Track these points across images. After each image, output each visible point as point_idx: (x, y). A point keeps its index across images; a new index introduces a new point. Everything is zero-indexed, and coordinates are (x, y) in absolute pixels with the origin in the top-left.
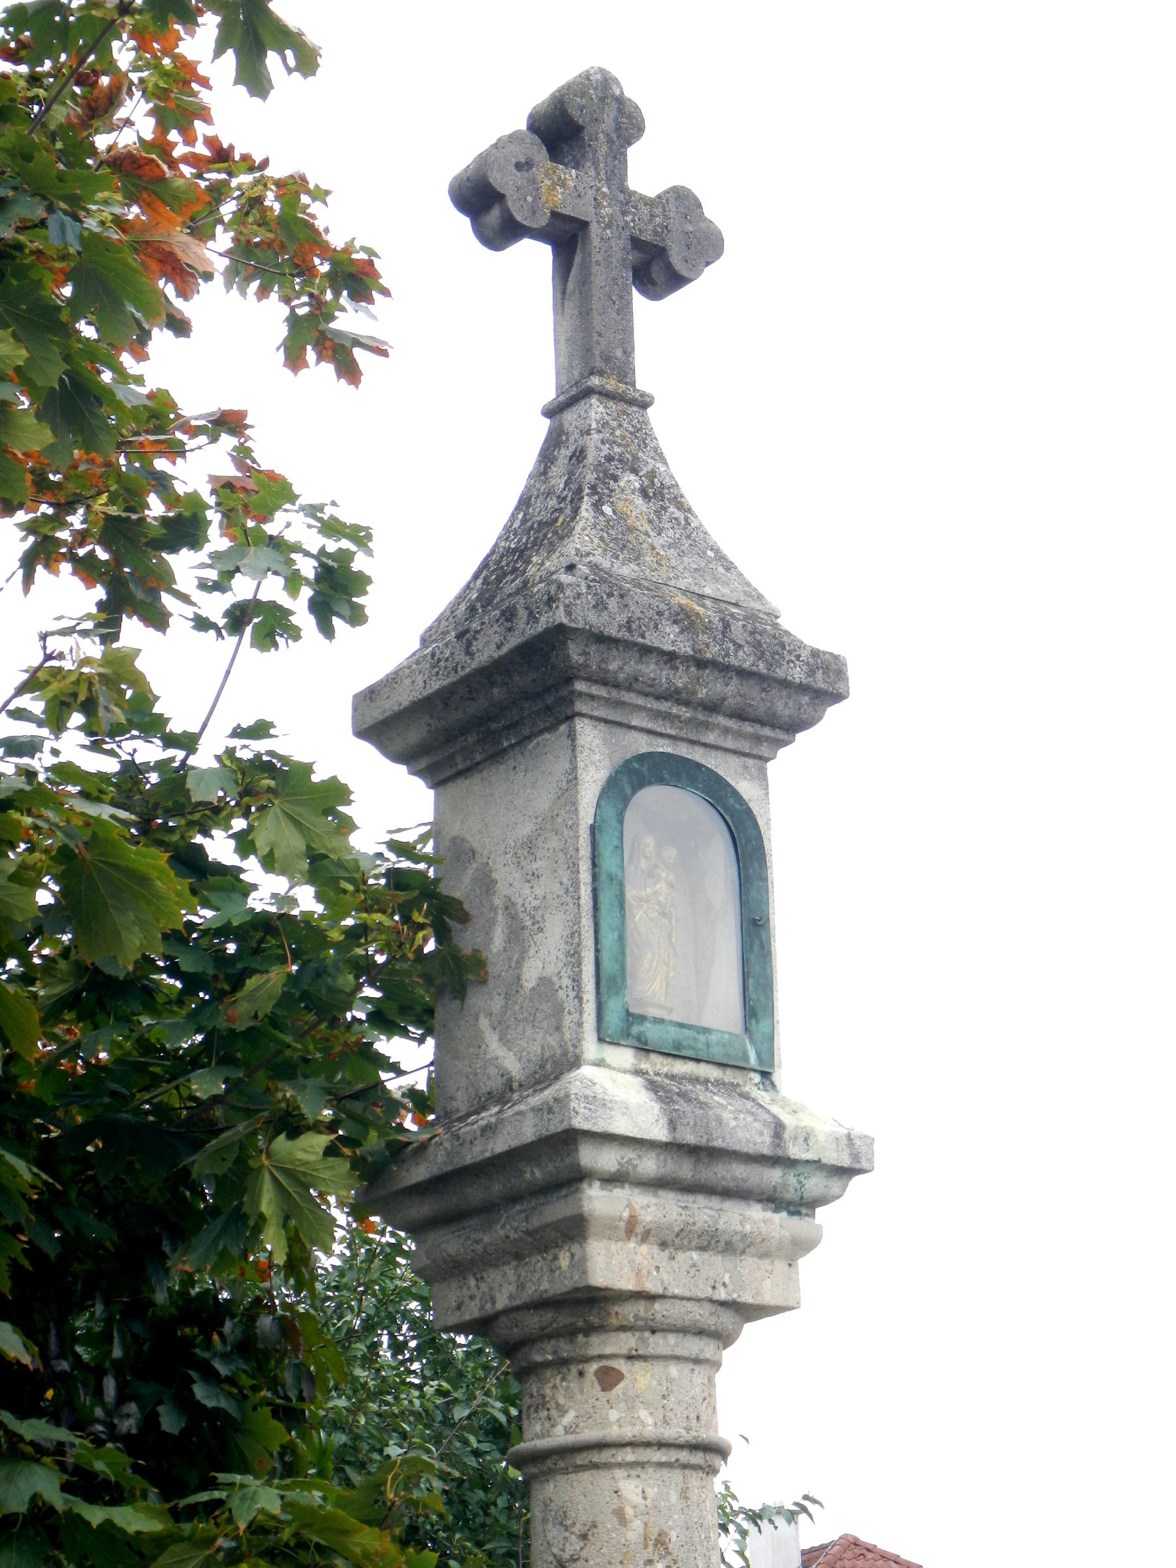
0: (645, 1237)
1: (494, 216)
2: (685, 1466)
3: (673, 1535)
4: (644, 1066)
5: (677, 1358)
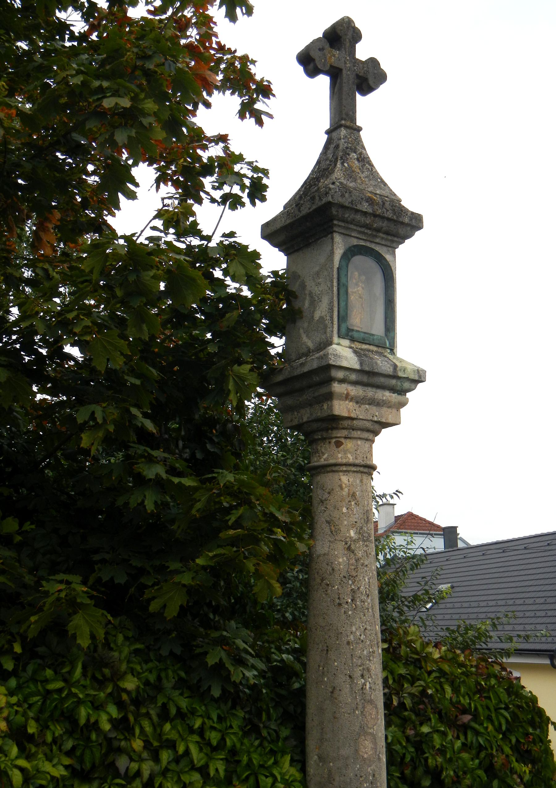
1: (311, 66)
2: (362, 472)
3: (357, 493)
4: (352, 346)
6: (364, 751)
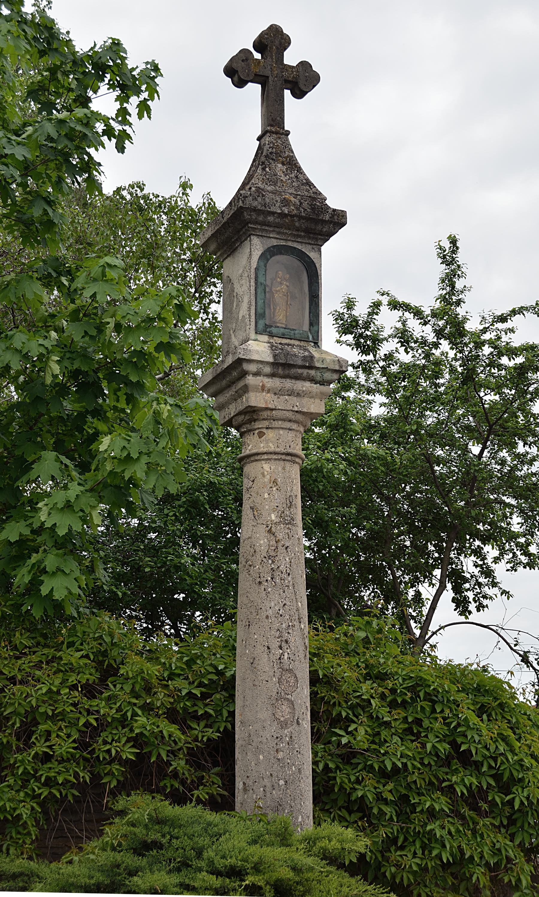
0: (269, 391)
1: (236, 78)
2: (284, 460)
3: (279, 480)
4: (271, 341)
5: (282, 428)
6: (280, 714)
